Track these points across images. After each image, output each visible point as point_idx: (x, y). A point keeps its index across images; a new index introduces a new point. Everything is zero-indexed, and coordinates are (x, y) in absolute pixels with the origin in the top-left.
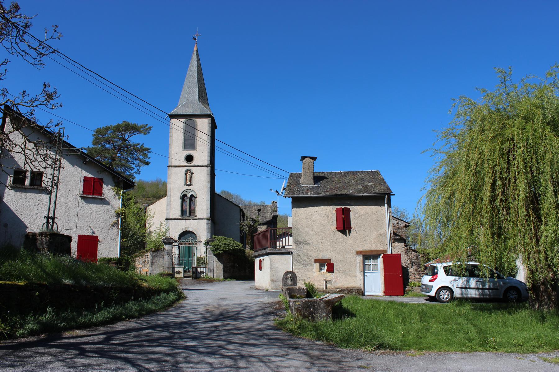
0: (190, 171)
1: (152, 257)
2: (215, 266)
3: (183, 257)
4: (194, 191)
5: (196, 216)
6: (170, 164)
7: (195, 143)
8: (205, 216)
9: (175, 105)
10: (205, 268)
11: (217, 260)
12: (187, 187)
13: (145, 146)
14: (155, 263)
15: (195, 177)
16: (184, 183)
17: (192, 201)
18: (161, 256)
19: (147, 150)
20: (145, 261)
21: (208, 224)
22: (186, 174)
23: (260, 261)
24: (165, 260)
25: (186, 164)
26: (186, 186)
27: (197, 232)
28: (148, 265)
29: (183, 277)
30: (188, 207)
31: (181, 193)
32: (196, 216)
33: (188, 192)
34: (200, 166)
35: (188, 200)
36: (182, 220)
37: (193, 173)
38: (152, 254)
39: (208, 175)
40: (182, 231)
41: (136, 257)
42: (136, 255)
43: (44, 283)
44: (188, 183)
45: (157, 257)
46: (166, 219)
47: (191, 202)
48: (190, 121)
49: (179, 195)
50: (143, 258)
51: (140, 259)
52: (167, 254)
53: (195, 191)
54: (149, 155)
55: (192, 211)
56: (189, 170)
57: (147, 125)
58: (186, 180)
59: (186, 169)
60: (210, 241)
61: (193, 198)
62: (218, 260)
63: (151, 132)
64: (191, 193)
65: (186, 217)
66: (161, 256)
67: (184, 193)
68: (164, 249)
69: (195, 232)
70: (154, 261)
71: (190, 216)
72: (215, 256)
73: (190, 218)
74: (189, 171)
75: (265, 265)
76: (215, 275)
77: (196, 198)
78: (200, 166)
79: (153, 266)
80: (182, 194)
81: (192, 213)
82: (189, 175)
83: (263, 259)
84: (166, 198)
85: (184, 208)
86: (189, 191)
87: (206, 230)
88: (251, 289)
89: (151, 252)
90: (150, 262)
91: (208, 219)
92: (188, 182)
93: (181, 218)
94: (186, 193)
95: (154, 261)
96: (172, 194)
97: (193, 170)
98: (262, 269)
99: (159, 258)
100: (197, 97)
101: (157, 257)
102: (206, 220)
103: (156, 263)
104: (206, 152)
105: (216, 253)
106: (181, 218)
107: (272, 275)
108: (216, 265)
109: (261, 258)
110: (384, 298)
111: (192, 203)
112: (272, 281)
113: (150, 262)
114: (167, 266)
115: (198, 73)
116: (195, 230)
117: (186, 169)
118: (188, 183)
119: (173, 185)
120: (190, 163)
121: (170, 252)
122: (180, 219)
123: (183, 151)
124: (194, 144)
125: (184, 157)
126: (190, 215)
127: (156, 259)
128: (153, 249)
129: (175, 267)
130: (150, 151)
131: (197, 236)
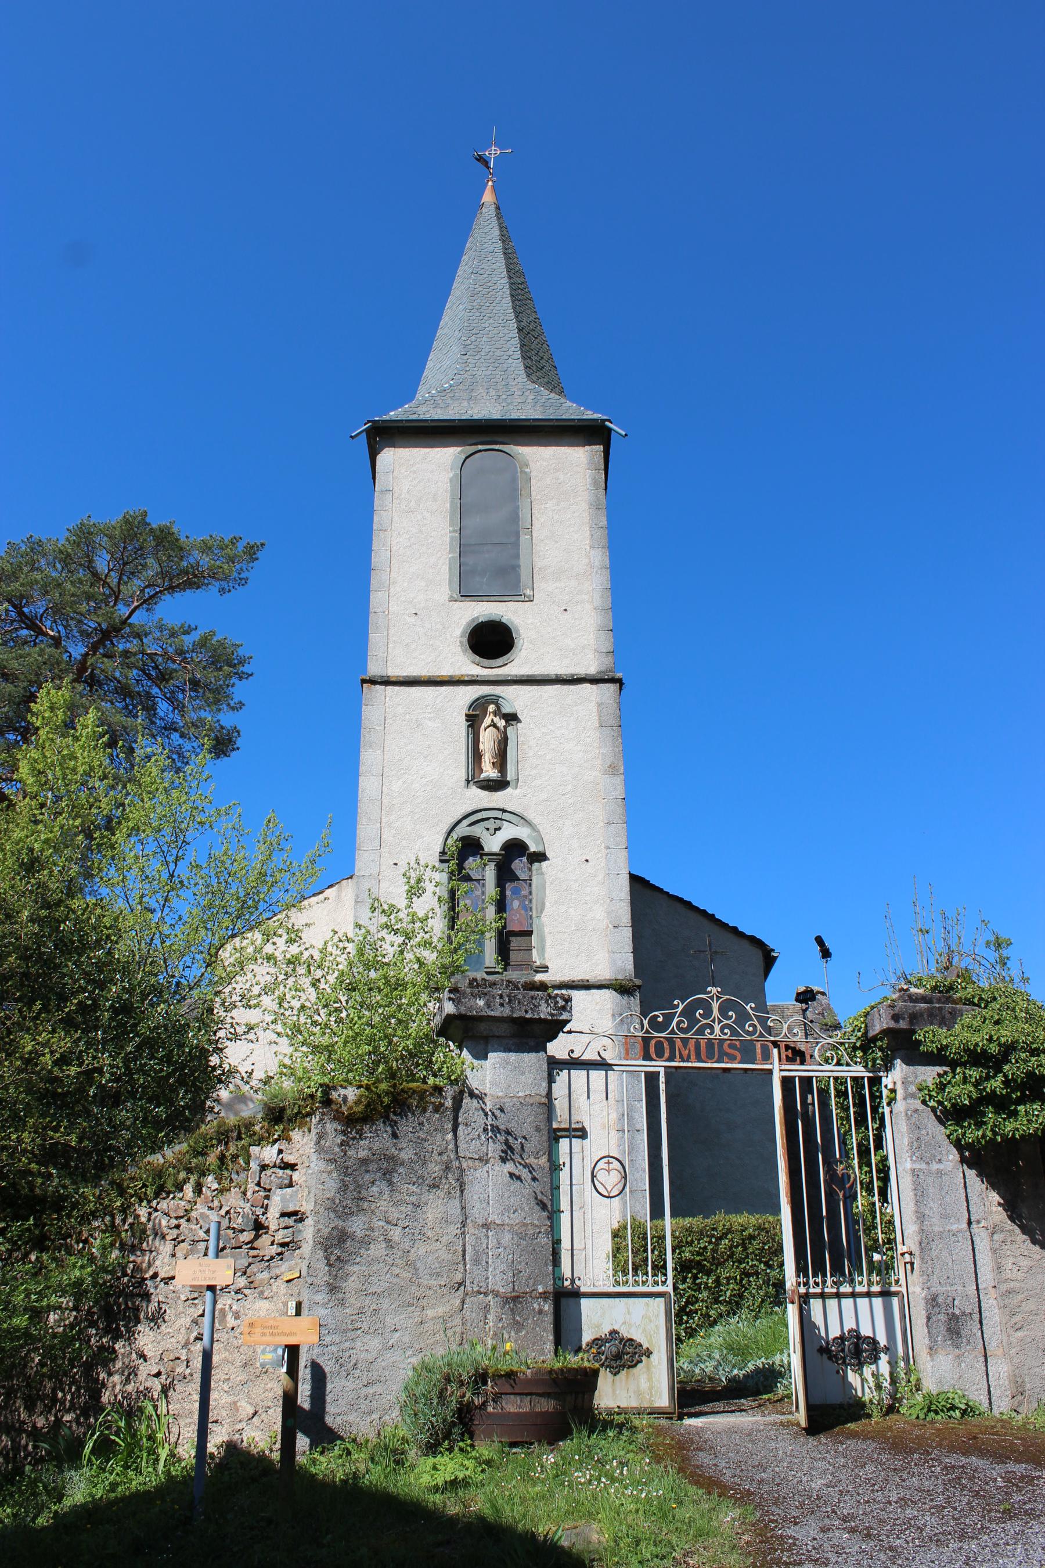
0: (498, 707)
1: (332, 1185)
2: (987, 1277)
6: (374, 669)
7: (523, 561)
8: (603, 972)
9: (409, 394)
10: (886, 1294)
11: (999, 1215)
14: (366, 1242)
16: (464, 776)
17: (515, 878)
18: (434, 1168)
20: (259, 1227)
22: (473, 720)
24: (477, 1213)
25: (468, 665)
26: (475, 791)
28: (287, 1269)
29: (663, 1400)
31: (446, 828)
32: (544, 969)
33: (491, 824)
35: (490, 874)
37: (512, 718)
39: (607, 731)
41: (161, 1191)
42: (159, 1174)
43: (751, 1367)
44: (489, 772)
45: (387, 1175)
47: (509, 886)
48: (488, 458)
50: (233, 1199)
51: (201, 1209)
52: (494, 1149)
53: (530, 816)
55: (515, 942)
56: (495, 700)
57: (234, 541)
58: (476, 755)
61: (519, 865)
62: (1012, 1208)
63: (256, 573)
64: (509, 832)
66: (434, 1168)
67: (463, 830)
68: (464, 1092)
70: (357, 1225)
72: (971, 1174)
74: (492, 708)
76: (1000, 1369)
77: (540, 857)
79: (351, 1285)
80: (455, 835)
81: (514, 957)
82: (494, 725)
89: (331, 1126)
90: (308, 1231)
91: (623, 989)
94: (478, 831)
95: (357, 1225)
99: (408, 1190)
101: (387, 1175)
102: (608, 995)
103: (378, 1249)
104: (588, 607)
105: (972, 1135)
108: (999, 1268)
111: (516, 892)
113: (308, 1231)
114: (498, 1278)
118: (489, 772)
120: (500, 661)
121: (525, 1124)
123: (452, 600)
124: (515, 568)
127: (383, 1204)
128: (351, 1093)
129: (576, 1295)
130: (246, 669)
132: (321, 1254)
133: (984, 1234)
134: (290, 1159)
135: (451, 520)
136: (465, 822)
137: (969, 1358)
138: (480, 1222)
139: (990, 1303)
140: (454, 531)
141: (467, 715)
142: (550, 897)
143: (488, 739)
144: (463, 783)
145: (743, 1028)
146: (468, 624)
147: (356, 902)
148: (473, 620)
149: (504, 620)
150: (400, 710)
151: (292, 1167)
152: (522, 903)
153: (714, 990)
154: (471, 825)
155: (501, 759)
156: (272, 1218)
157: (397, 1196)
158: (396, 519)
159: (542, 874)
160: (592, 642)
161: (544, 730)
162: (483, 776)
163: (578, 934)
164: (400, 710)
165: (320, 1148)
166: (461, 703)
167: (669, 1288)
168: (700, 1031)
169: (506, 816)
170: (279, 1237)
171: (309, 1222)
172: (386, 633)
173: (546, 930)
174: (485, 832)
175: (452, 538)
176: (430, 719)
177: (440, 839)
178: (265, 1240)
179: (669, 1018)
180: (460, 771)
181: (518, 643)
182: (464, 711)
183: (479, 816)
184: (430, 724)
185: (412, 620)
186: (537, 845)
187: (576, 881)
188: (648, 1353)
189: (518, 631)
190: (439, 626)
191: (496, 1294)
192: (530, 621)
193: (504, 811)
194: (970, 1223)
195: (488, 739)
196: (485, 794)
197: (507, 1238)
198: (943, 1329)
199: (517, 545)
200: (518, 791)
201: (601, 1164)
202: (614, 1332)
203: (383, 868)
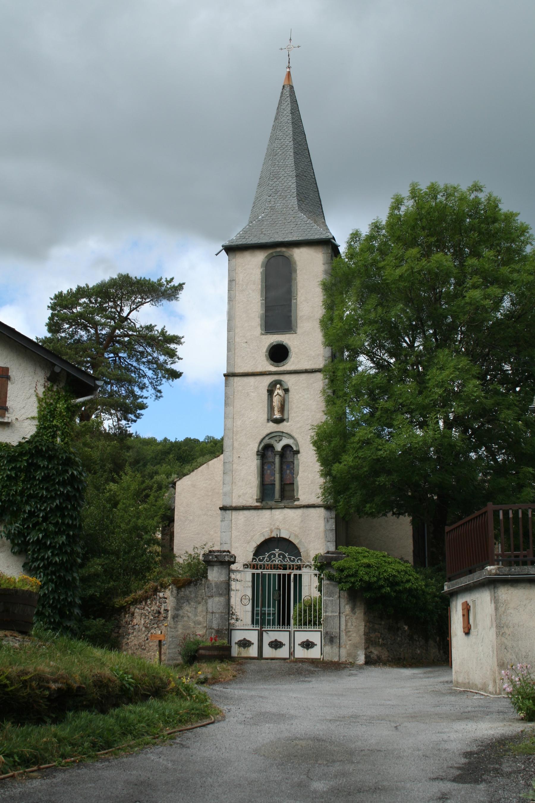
0: (281, 385)
2: (343, 627)
3: (269, 607)
4: (290, 436)
5: (298, 499)
8: (319, 501)
12: (272, 427)
13: (171, 332)
14: (183, 617)
15: (293, 396)
19: (176, 340)
20: (159, 613)
21: (327, 520)
22: (270, 392)
23: (467, 609)
26: (271, 424)
27: (300, 541)
30: (277, 476)
33: (277, 439)
34: (306, 372)
35: (277, 460)
36: (262, 508)
38: (175, 592)
40: (262, 539)
44: (277, 415)
45: (188, 601)
46: (221, 509)
49: (254, 447)
54: (180, 350)
55: (287, 488)
56: (279, 382)
58: (271, 408)
59: (268, 380)
60: (332, 559)
64: (285, 441)
65: (271, 503)
67: (266, 441)
69: (295, 542)
71: (282, 500)
73: (282, 505)
74: (278, 386)
75: (479, 617)
78: (306, 372)
80: (262, 444)
82: (278, 394)
83: (474, 601)
84: (222, 456)
85: (268, 480)
86: (280, 435)
87: (322, 535)
88: (451, 693)
92: (276, 412)
93: (258, 504)
94: (272, 442)
96: (236, 444)
97: (289, 381)
98: (473, 630)
100: (294, 201)
106: (258, 504)
107: (502, 648)
108: (346, 625)
109: (468, 598)
110: (511, 728)
112: (502, 665)
115: (294, 140)
116: (296, 536)
117: (268, 380)
119: (239, 423)
120: (282, 364)
122: (256, 508)
123: (262, 334)
125: (265, 350)
126: (283, 497)
131: (301, 550)
132: (172, 620)
133: (344, 617)
134: (166, 596)
135: (261, 294)
136: (267, 438)
137: (335, 647)
138: (211, 611)
139: (343, 634)
140: (263, 300)
141: (268, 390)
142: (301, 469)
143: (276, 401)
144: (266, 421)
145: (284, 561)
146: (269, 346)
147: (224, 473)
148: (271, 344)
149: (284, 344)
150: (240, 388)
151: (166, 598)
152: (290, 471)
153: (277, 550)
154: (269, 439)
155: (282, 409)
156: (162, 611)
157: (190, 606)
158: (237, 294)
159: (298, 459)
160: (322, 352)
161: (300, 395)
162: (275, 417)
163: (312, 485)
164: (240, 388)
165: (172, 595)
166: (266, 384)
167: (259, 628)
168: (272, 561)
169: (284, 435)
170: (163, 615)
171: (170, 612)
172: (233, 352)
173: (299, 483)
174: (275, 442)
175: (262, 303)
176: (252, 392)
177: (257, 445)
178: (161, 616)
179: (264, 558)
180: (265, 416)
181: (290, 354)
182: (267, 388)
183: (273, 435)
184: (252, 394)
185: (245, 345)
186: (296, 447)
187: (311, 462)
188: (253, 644)
189: (290, 348)
190: (256, 348)
191: (214, 629)
192: (295, 343)
193: (283, 432)
194: (340, 613)
195: (276, 401)
196: (275, 425)
197: (217, 615)
198: (328, 640)
199: (290, 306)
200: (288, 424)
201: (244, 597)
202: (276, 640)
203: (234, 458)
